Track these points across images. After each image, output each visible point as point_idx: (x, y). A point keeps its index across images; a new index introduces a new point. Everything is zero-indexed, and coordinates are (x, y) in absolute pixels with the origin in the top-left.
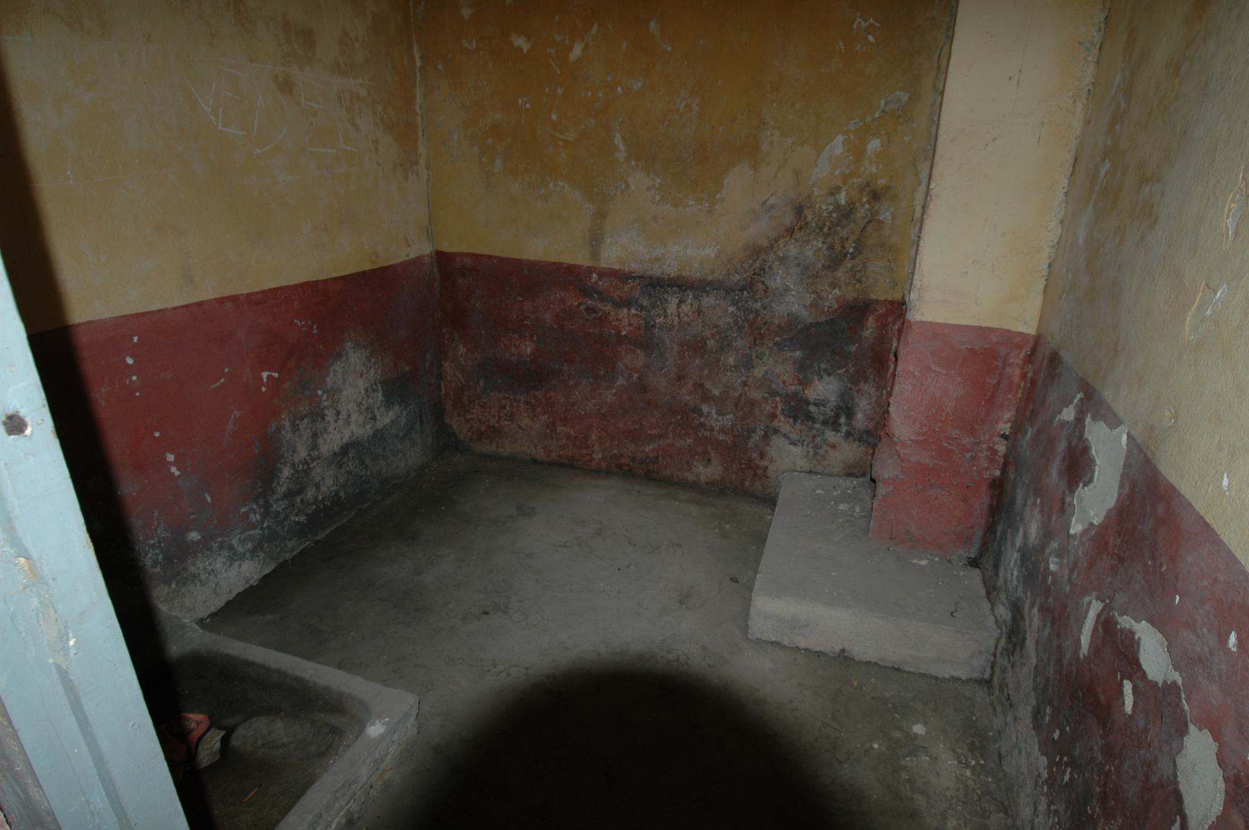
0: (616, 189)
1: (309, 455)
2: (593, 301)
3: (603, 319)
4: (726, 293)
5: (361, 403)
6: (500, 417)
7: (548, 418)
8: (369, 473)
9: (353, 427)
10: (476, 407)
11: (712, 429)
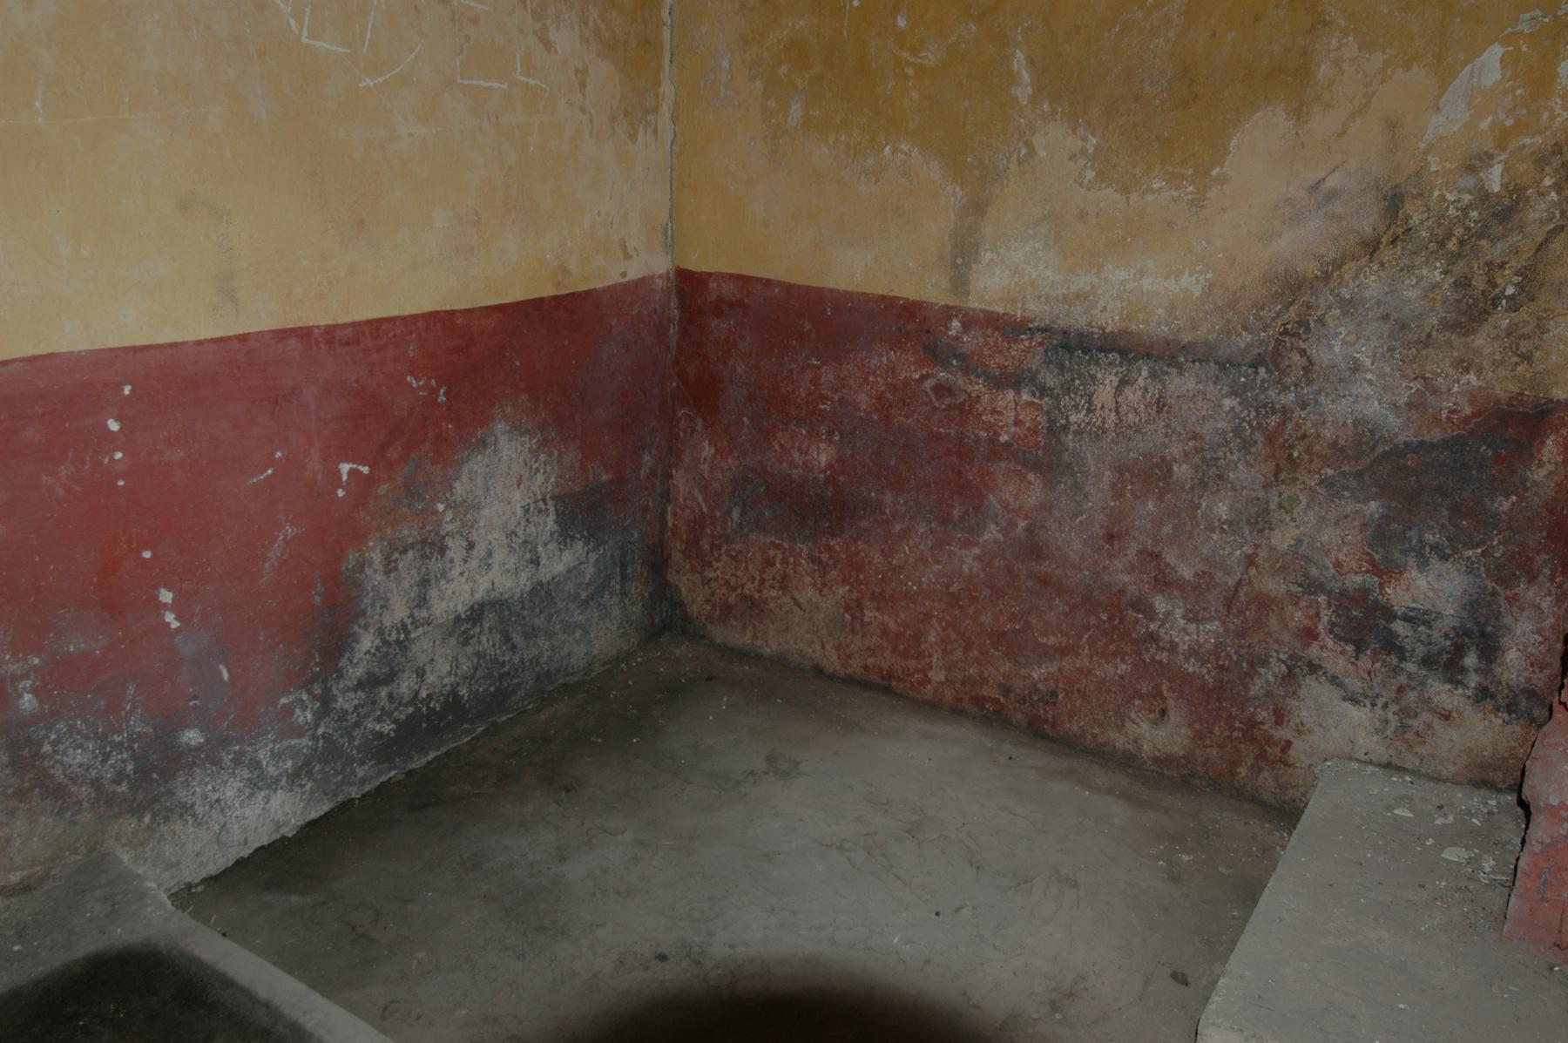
0: (1009, 158)
1: (411, 616)
2: (948, 372)
3: (967, 409)
4: (1221, 370)
5: (514, 533)
6: (762, 582)
7: (850, 591)
8: (516, 660)
9: (495, 573)
10: (724, 558)
11: (1173, 647)
